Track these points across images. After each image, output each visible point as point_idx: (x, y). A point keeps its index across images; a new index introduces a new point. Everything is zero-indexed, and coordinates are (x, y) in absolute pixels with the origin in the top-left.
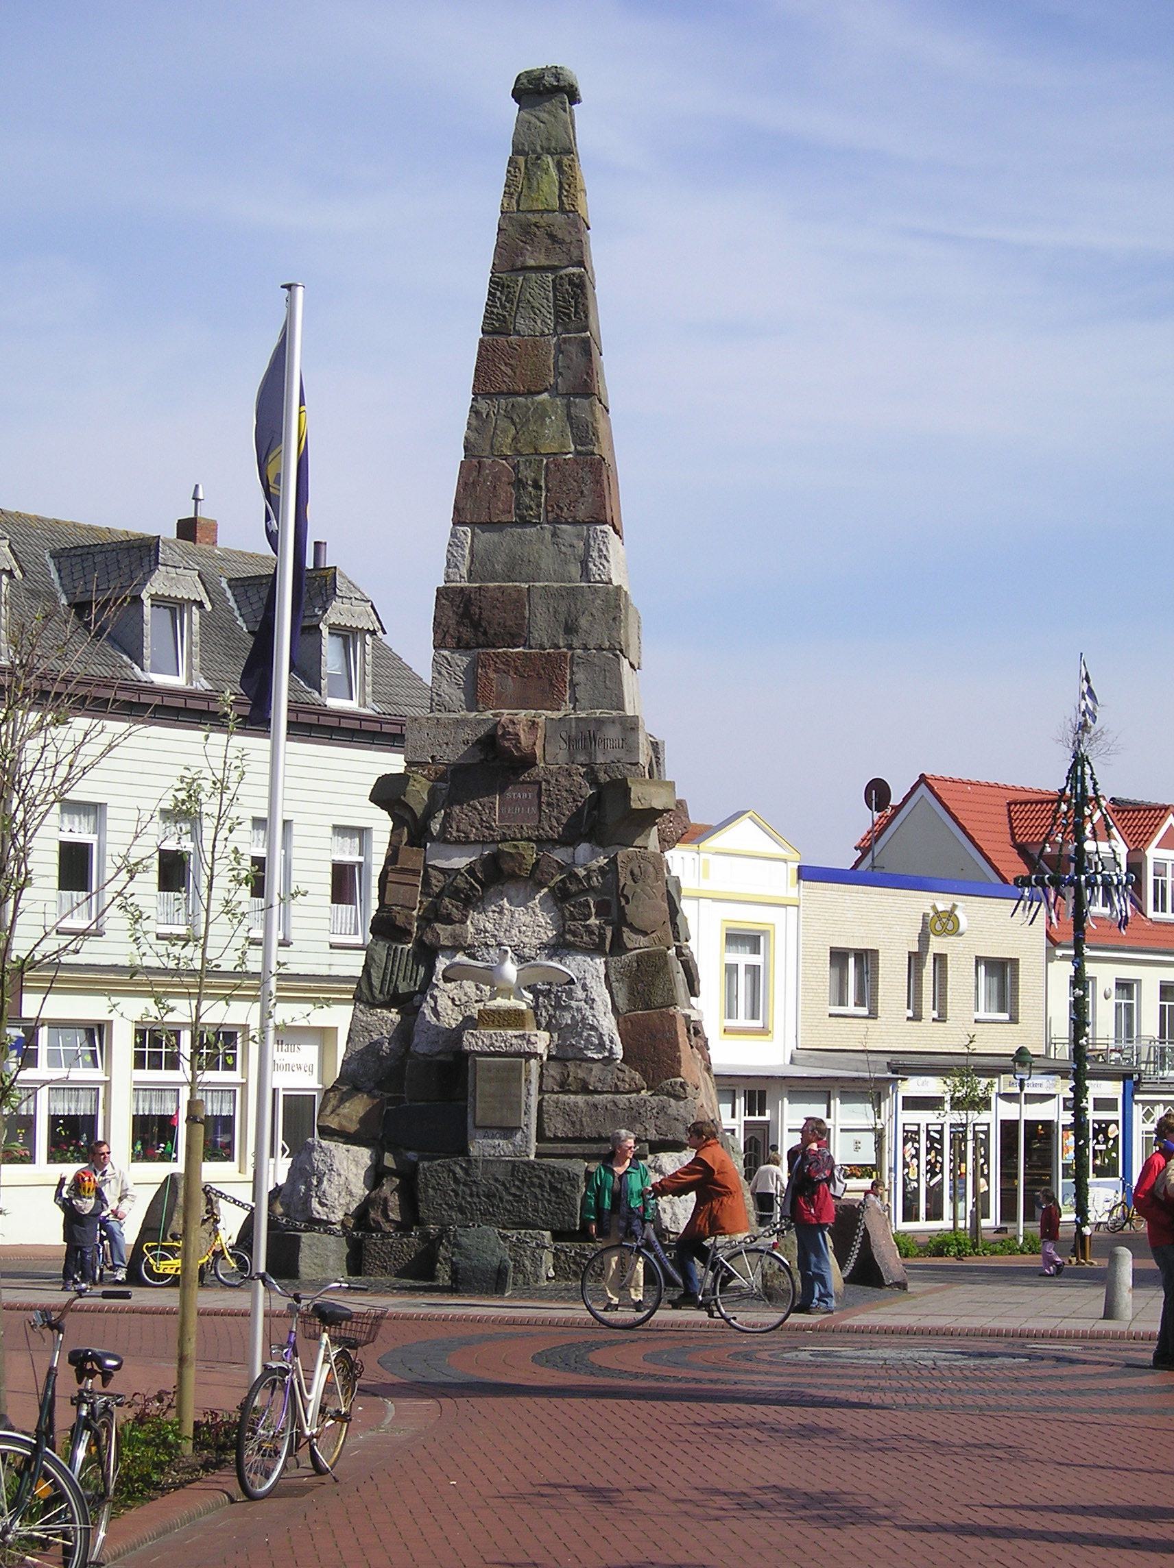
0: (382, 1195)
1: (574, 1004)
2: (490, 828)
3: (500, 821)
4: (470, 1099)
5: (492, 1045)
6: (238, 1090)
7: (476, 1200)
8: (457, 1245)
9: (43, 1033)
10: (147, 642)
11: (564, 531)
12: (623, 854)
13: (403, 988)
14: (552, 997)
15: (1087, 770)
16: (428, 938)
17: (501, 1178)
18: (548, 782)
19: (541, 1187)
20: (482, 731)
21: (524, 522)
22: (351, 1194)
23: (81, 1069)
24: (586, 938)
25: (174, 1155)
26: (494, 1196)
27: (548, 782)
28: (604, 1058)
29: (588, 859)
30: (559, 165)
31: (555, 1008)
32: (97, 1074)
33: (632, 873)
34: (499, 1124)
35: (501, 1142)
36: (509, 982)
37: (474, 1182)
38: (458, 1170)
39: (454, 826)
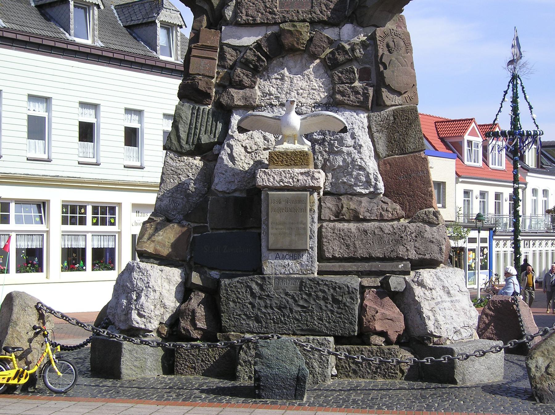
0: (191, 307)
1: (345, 149)
3: (280, 8)
4: (263, 226)
5: (282, 181)
6: (117, 235)
7: (270, 311)
8: (258, 355)
9: (12, 206)
10: (72, 22)
12: (379, 32)
13: (205, 139)
14: (327, 143)
15: (519, 82)
16: (225, 100)
17: (291, 292)
19: (325, 299)
22: (165, 307)
23: (34, 225)
24: (352, 97)
25: (84, 268)
26: (285, 307)
28: (370, 193)
29: (351, 35)
31: (329, 153)
32: (42, 227)
33: (388, 46)
34: (289, 248)
35: (290, 262)
36: (294, 129)
37: (268, 296)
38: (254, 286)
39: (244, 11)
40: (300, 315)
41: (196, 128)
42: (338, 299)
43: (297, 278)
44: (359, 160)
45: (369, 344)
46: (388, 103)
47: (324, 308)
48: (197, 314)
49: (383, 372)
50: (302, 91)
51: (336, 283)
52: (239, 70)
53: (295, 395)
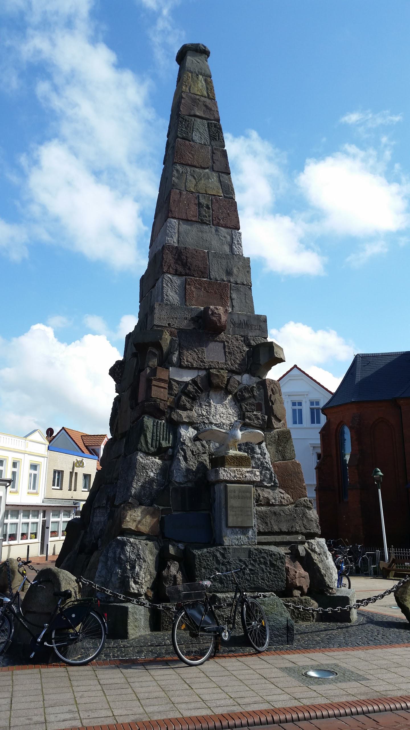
1: (256, 456)
2: (202, 362)
5: (235, 476)
11: (221, 230)
16: (175, 417)
18: (228, 342)
19: (265, 563)
20: (194, 314)
21: (203, 223)
24: (256, 421)
27: (228, 342)
30: (206, 81)
33: (272, 390)
37: (228, 562)
38: (218, 555)
40: (250, 576)
41: (157, 436)
42: (273, 563)
43: (247, 548)
44: (265, 463)
45: (292, 596)
46: (275, 426)
47: (265, 570)
48: (178, 579)
49: (302, 617)
50: (222, 415)
51: (272, 551)
52: (183, 398)
53: (288, 641)
